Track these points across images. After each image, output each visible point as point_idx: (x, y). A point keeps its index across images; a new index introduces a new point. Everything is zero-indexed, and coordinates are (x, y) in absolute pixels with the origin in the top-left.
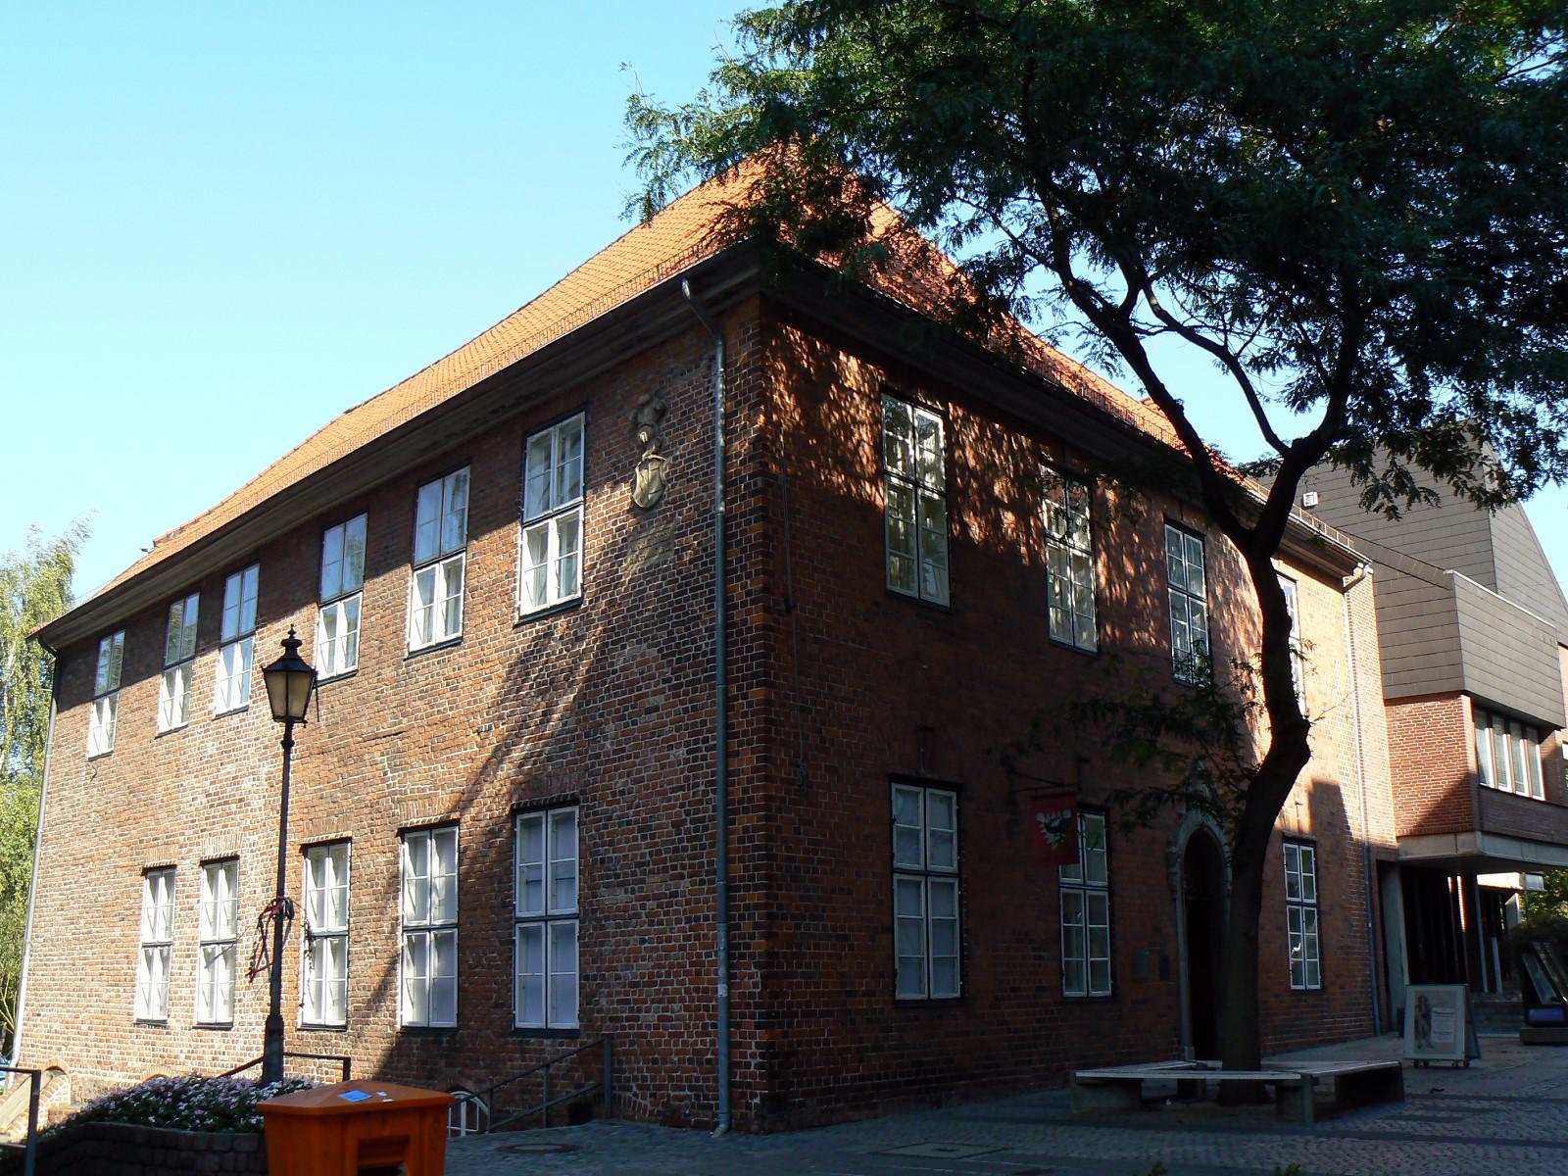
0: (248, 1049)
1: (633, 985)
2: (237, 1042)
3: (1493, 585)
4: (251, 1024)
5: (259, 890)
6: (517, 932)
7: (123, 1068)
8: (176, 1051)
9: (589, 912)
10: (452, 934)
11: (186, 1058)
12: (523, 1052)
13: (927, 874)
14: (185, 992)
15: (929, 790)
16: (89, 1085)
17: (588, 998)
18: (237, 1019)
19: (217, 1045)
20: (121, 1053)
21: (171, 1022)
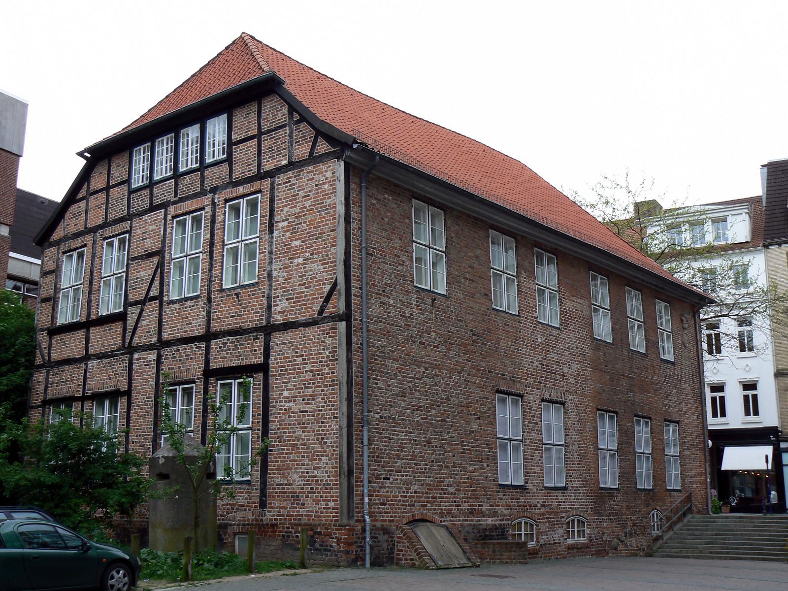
0: (577, 499)
1: (692, 477)
2: (571, 496)
3: (77, 154)
4: (577, 487)
5: (576, 423)
6: (163, 439)
7: (495, 514)
8: (534, 502)
9: (681, 456)
10: (249, 433)
11: (542, 506)
12: (670, 496)
13: (554, 445)
14: (537, 470)
15: (510, 397)
16: (470, 529)
17: (683, 480)
18: (570, 485)
19: (560, 498)
20: (491, 506)
21: (530, 486)
